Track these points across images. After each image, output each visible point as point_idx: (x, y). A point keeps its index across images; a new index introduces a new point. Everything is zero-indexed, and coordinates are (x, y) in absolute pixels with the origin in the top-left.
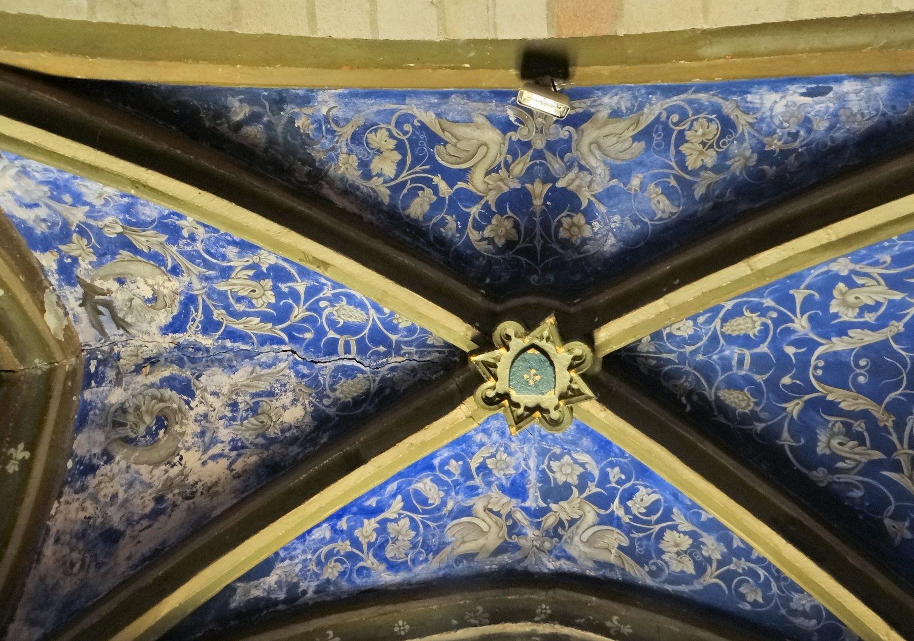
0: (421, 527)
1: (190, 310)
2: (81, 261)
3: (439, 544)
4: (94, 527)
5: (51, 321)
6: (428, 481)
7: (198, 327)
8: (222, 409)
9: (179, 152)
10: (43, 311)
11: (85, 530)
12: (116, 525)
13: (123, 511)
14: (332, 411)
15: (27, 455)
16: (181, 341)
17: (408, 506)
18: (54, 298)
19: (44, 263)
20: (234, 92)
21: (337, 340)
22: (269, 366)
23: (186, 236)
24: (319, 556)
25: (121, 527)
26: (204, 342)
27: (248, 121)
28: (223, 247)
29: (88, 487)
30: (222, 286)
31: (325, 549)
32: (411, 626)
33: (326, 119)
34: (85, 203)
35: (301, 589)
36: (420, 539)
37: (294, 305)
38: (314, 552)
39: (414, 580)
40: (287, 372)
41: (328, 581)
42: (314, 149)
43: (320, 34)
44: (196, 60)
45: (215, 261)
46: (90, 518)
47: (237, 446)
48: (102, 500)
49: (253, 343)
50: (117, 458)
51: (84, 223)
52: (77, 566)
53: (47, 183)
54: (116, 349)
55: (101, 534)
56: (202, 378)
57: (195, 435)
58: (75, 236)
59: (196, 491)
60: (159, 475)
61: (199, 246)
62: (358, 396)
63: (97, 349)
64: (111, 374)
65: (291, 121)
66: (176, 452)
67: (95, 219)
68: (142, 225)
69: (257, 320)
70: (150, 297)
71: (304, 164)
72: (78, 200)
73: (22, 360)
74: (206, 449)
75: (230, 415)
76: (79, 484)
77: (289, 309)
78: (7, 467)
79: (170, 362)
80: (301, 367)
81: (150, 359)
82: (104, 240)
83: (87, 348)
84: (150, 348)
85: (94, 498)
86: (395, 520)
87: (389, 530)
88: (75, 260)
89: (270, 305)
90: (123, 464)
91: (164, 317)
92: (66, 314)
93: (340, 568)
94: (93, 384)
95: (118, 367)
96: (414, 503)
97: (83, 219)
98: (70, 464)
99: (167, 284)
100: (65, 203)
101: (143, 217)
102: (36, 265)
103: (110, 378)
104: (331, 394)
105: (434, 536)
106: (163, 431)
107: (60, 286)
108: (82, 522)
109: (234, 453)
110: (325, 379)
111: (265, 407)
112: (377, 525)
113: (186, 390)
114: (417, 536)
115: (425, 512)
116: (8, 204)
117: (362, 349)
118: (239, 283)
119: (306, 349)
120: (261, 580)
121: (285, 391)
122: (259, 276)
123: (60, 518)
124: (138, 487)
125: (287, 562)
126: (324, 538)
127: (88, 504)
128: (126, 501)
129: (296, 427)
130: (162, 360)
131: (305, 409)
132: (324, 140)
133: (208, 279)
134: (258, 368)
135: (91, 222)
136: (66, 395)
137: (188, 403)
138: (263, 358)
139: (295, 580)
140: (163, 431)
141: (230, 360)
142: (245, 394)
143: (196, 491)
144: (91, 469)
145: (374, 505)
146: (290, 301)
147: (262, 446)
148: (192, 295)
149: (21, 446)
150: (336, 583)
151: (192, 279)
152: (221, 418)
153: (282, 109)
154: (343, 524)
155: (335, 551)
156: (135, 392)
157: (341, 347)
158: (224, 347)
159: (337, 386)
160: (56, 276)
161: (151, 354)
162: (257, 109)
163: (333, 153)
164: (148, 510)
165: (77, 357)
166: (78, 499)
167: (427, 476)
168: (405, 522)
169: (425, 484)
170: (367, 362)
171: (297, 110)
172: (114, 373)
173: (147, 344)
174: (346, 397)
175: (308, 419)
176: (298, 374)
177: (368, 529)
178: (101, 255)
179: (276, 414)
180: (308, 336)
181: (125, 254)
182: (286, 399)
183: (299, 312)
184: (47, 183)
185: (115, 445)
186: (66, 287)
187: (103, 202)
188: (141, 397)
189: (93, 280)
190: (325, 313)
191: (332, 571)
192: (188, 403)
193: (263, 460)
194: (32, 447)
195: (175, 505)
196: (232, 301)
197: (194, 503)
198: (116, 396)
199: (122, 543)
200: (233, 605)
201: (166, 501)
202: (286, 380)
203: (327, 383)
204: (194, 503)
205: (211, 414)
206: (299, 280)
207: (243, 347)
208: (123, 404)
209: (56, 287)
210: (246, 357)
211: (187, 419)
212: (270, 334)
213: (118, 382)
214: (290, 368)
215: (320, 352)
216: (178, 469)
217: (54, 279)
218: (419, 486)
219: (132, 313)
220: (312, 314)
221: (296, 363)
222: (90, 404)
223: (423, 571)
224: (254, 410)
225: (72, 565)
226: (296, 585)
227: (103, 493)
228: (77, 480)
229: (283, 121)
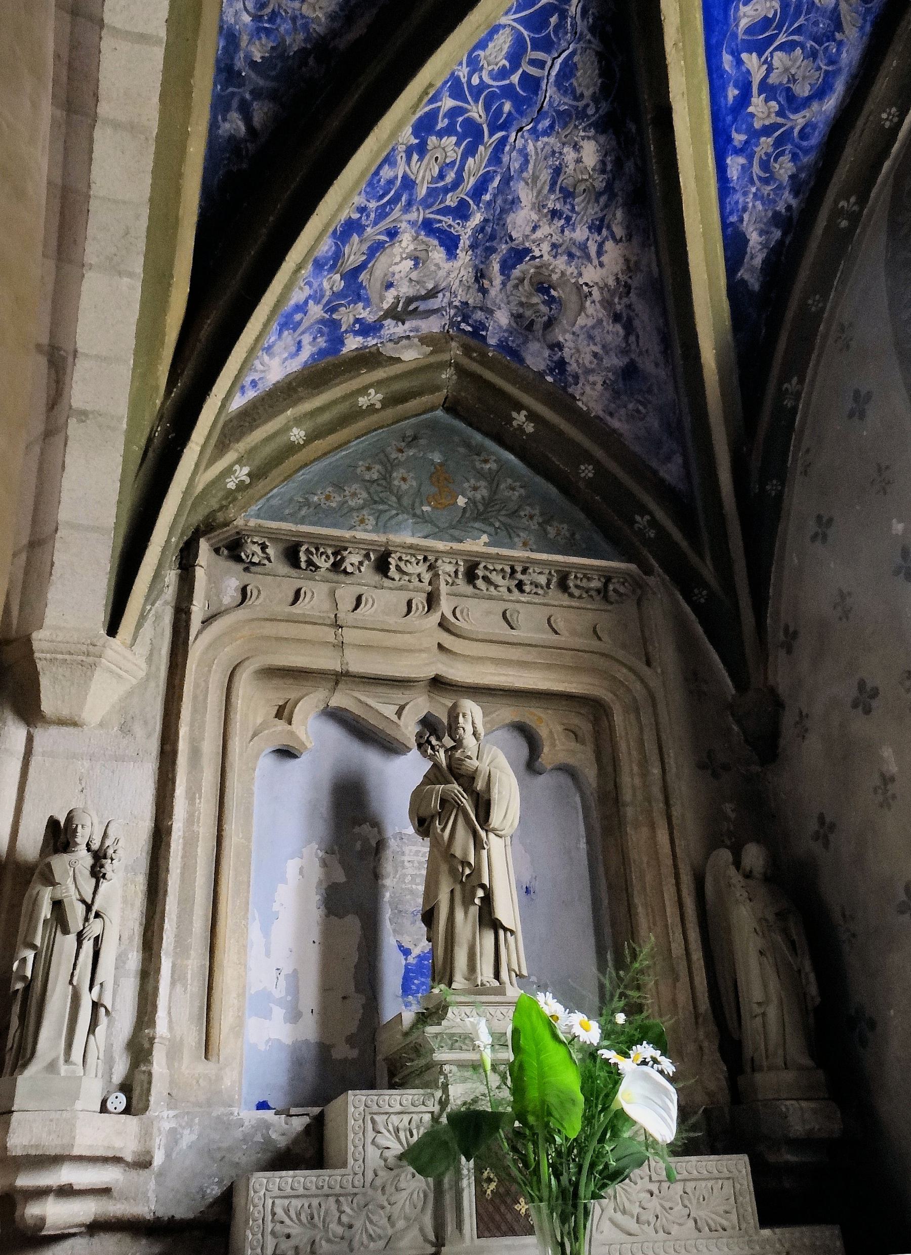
0: (796, 38)
1: (439, 228)
2: (361, 317)
3: (831, 19)
4: (613, 382)
5: (411, 355)
6: (743, 9)
7: (458, 224)
8: (554, 227)
9: (271, 218)
10: (399, 360)
11: (613, 390)
12: (621, 364)
13: (612, 354)
14: (605, 107)
15: (524, 413)
16: (468, 243)
17: (759, 48)
18: (390, 345)
19: (354, 347)
20: (213, 126)
21: (525, 75)
22: (527, 162)
23: (358, 215)
24: (760, 178)
25: (626, 360)
26: (477, 221)
27: (247, 118)
28: (379, 181)
29: (576, 373)
30: (422, 191)
31: (756, 169)
32: (894, 105)
33: (257, 18)
34: (306, 302)
35: (783, 211)
36: (810, 43)
37: (466, 115)
38: (752, 182)
39: (854, 71)
40: (540, 144)
41: (792, 177)
42: (290, 45)
43: (163, 34)
44: (180, 175)
45: (392, 193)
46: (604, 382)
47: (597, 227)
48: (593, 366)
49: (495, 172)
50: (561, 339)
51: (324, 307)
52: (641, 408)
53: (280, 332)
54: (457, 303)
55: (624, 379)
56: (514, 235)
57: (569, 263)
58: (334, 316)
59: (626, 282)
60: (593, 310)
61: (373, 205)
62: (600, 69)
63: (451, 319)
64: (479, 315)
65: (253, 64)
66: (578, 287)
67: (322, 296)
68: (338, 255)
69: (470, 160)
70: (413, 262)
71: (306, 64)
72: (301, 308)
73: (438, 389)
74: (588, 258)
75: (562, 222)
76: (570, 379)
77: (469, 122)
78: (527, 432)
79: (486, 259)
80: (540, 127)
81: (476, 277)
82: (345, 292)
83: (447, 327)
84: (466, 274)
85: (588, 372)
86: (770, 70)
87: (777, 82)
88: (357, 320)
89: (458, 144)
90: (568, 336)
91: (438, 255)
92: (408, 337)
93: (786, 159)
94: (484, 333)
95: (475, 308)
96: (760, 39)
97: (320, 306)
98: (549, 379)
99: (404, 244)
100: (302, 319)
101: (330, 254)
102: (355, 353)
103: (483, 317)
104: (584, 102)
105: (816, 23)
106: (552, 291)
107: (380, 337)
108: (606, 389)
109: (605, 232)
110: (564, 103)
111: (570, 181)
112: (764, 95)
113: (520, 254)
114: (803, 48)
115: (779, 27)
116: (294, 364)
117: (545, 45)
118: (424, 173)
119: (521, 113)
120: (748, 250)
121: (561, 153)
122: (421, 149)
123: (592, 405)
124: (596, 332)
125: (746, 217)
126: (743, 166)
127: (591, 378)
128: (604, 347)
129: (605, 156)
130: (481, 266)
131: (589, 138)
132: (282, 29)
133: (409, 204)
134: (525, 175)
135: (324, 301)
136: (484, 361)
137: (534, 258)
138: (515, 165)
139: (770, 214)
140: (552, 291)
141: (505, 201)
142: (547, 198)
143: (626, 282)
144: (561, 365)
145: (736, 92)
146: (460, 119)
147: (610, 199)
148: (423, 222)
149: (514, 414)
150: (800, 170)
151: (406, 220)
152: (562, 232)
153: (239, 73)
154: (739, 138)
155: (764, 158)
156: (505, 300)
157: (533, 71)
158: (489, 204)
159: (578, 92)
160: (369, 339)
161: (472, 275)
162: (235, 103)
163: (299, 22)
164: (621, 332)
165: (452, 339)
166: (583, 384)
167: (737, 9)
168: (779, 59)
169: (745, 15)
170: (564, 44)
171: (242, 55)
172: (479, 313)
173: (460, 276)
174: (595, 85)
175: (602, 139)
176: (547, 132)
177: (761, 109)
178: (358, 298)
179: (582, 173)
180: (507, 107)
181: (363, 277)
182: (570, 155)
183: (477, 112)
184: (280, 332)
185: (548, 337)
186: (382, 332)
187: (307, 287)
188: (512, 298)
189: (381, 309)
190: (486, 79)
191: (784, 168)
192: (534, 258)
193: (624, 205)
194: (519, 407)
195: (629, 307)
196: (441, 184)
197: (636, 288)
198: (502, 318)
199: (640, 365)
200: (756, 287)
201: (621, 313)
202: (548, 149)
203: (571, 102)
204: (636, 288)
205: (554, 240)
206: (439, 104)
207: (496, 183)
208: (512, 315)
209: (379, 341)
210: (508, 183)
211: (550, 265)
212: (490, 150)
213: (490, 312)
214: (537, 140)
215: (531, 98)
216: (596, 292)
217: (371, 341)
218: (744, 23)
219: (425, 282)
220: (483, 96)
221: (533, 131)
222: (502, 342)
223: (849, 56)
224: (567, 194)
225: (638, 411)
226: (776, 214)
227: (587, 364)
228: (566, 378)
229: (253, 75)
